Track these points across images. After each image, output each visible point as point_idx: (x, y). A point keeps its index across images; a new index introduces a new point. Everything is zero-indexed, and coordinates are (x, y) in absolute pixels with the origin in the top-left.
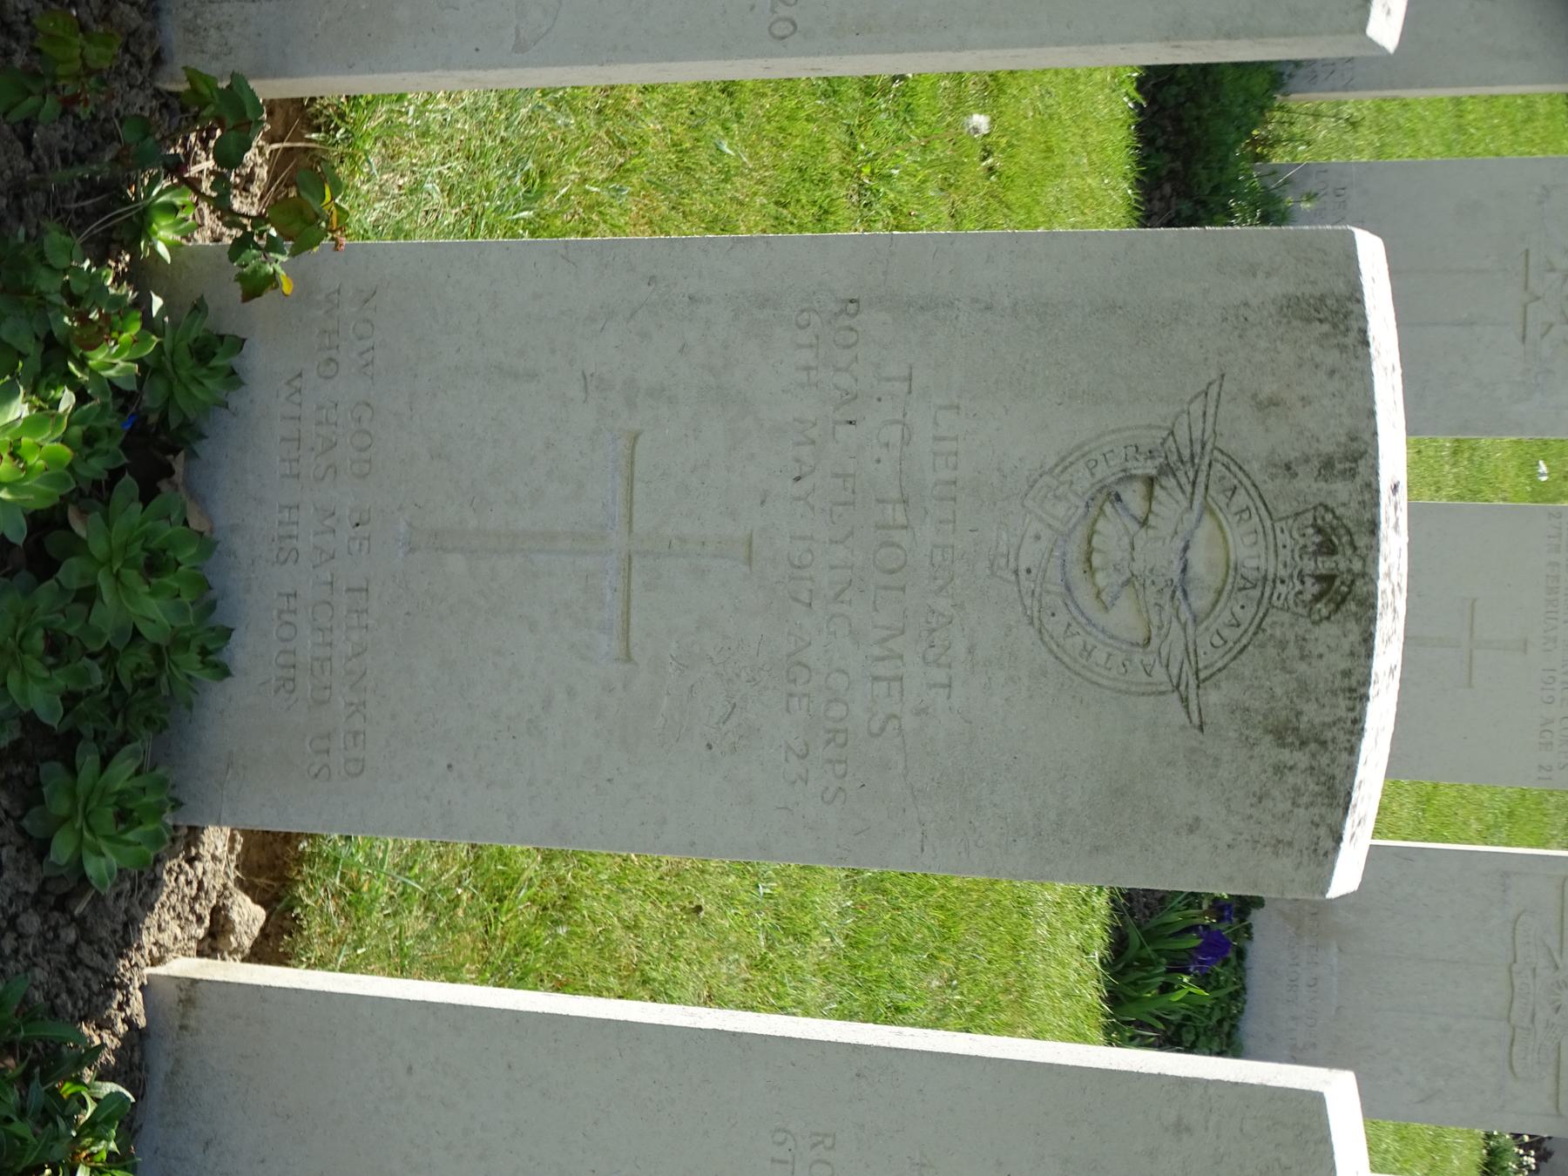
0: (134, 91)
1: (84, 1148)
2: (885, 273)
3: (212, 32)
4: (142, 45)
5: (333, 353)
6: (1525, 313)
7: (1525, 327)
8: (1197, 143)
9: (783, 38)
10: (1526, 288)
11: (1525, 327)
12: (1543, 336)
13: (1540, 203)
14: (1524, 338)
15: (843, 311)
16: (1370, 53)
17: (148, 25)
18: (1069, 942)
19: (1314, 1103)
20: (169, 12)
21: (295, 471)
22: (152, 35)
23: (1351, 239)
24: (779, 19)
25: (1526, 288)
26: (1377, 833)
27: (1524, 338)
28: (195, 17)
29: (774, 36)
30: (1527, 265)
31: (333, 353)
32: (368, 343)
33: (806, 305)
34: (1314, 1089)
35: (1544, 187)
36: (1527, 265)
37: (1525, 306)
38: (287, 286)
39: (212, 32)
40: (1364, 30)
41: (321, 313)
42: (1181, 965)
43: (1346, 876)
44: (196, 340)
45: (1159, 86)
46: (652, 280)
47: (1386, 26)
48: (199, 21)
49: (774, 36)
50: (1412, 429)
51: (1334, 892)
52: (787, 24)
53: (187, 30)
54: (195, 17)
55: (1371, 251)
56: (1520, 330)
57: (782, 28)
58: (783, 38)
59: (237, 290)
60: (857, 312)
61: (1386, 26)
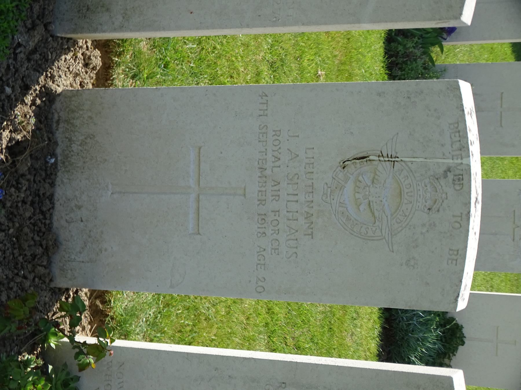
0: (43, 292)
2: (295, 375)
3: (69, 271)
4: (45, 277)
5: (110, 382)
6: (514, 231)
7: (514, 236)
8: (409, 54)
9: (260, 292)
10: (514, 223)
11: (514, 236)
14: (514, 240)
15: (280, 386)
16: (464, 25)
17: (48, 271)
20: (55, 263)
22: (49, 274)
23: (458, 82)
24: (259, 286)
25: (514, 223)
26: (471, 290)
27: (514, 240)
28: (64, 265)
29: (257, 292)
31: (110, 382)
32: (121, 380)
33: (268, 383)
36: (514, 216)
37: (514, 229)
38: (93, 366)
39: (69, 271)
40: (460, 18)
41: (106, 368)
43: (462, 305)
44: (63, 381)
45: (392, 38)
46: (216, 369)
48: (65, 267)
49: (257, 292)
50: (476, 269)
51: (458, 310)
52: (262, 288)
53: (61, 270)
54: (64, 265)
55: (466, 88)
57: (260, 289)
58: (260, 292)
59: (77, 368)
60: (285, 387)
61: (467, 16)
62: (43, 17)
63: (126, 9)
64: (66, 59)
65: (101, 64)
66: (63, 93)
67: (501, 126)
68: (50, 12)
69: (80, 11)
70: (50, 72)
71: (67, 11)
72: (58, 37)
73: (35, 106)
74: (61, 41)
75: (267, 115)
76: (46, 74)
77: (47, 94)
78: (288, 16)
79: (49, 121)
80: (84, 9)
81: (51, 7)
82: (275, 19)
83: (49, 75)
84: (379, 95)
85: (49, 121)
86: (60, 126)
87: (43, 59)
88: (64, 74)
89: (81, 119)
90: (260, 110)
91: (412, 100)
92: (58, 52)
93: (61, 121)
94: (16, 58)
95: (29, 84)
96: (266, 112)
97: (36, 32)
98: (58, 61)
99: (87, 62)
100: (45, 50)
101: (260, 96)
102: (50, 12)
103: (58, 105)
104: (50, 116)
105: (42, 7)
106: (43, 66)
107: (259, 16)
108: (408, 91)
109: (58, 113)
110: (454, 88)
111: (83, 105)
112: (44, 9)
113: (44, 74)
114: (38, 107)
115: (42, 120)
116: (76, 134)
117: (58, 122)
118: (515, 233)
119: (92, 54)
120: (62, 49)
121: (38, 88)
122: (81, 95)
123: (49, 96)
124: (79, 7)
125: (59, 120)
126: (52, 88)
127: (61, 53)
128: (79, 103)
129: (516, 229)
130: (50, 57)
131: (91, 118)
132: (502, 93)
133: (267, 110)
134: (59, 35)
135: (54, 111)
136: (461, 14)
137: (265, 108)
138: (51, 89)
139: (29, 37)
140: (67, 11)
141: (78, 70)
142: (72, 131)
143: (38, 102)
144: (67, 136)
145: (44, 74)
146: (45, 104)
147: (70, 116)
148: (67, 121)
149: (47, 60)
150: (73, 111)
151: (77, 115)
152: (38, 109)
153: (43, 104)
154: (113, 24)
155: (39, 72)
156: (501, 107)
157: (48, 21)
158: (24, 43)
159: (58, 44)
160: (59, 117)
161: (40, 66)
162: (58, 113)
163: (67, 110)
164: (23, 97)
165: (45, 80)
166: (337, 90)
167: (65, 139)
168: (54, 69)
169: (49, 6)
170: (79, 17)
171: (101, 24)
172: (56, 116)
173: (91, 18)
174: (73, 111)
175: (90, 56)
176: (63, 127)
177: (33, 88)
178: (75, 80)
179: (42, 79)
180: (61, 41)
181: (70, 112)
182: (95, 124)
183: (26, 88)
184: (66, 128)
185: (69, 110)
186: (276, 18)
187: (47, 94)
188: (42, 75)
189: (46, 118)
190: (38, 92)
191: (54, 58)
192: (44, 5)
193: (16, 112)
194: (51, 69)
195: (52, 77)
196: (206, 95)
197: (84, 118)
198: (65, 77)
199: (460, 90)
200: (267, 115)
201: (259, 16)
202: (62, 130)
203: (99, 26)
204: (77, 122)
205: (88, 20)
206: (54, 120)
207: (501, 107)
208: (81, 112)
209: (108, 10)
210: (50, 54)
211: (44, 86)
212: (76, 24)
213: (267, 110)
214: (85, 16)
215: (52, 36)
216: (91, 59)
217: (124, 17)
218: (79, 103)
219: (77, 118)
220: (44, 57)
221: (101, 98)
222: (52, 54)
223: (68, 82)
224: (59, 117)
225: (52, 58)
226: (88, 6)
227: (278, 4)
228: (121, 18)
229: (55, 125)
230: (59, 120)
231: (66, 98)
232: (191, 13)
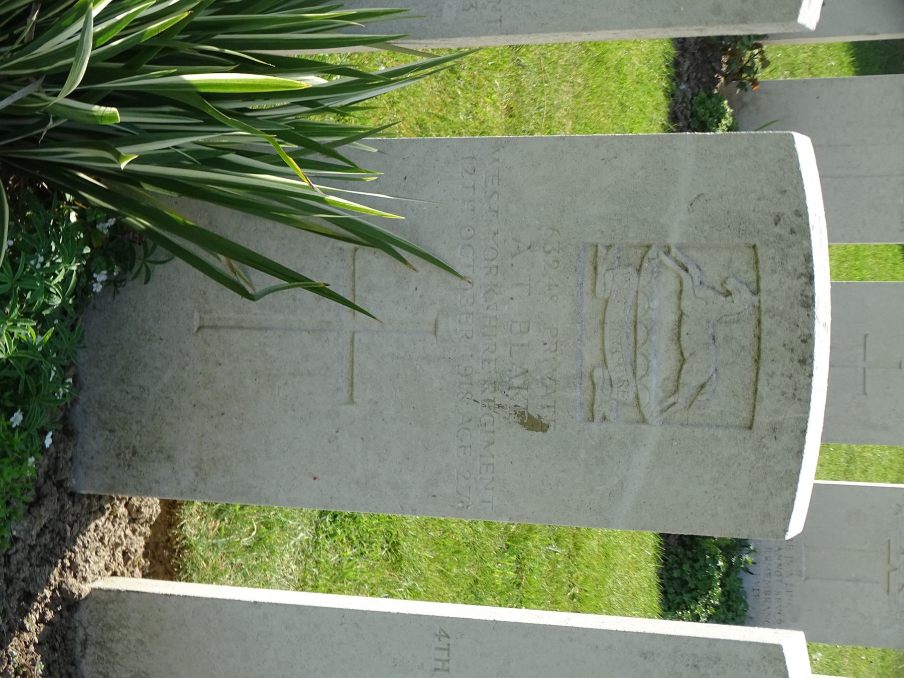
1: (177, 543)
8: (709, 80)
10: (889, 562)
12: (899, 591)
13: (896, 514)
18: (637, 561)
19: (774, 656)
21: (445, 668)
23: (792, 141)
26: (817, 477)
30: (889, 549)
34: (776, 643)
35: (898, 505)
36: (889, 549)
37: (889, 573)
42: (695, 573)
43: (796, 526)
47: (810, 15)
50: (831, 238)
51: (789, 536)
55: (803, 145)
56: (886, 587)
61: (810, 15)
62: (55, 473)
63: (201, 460)
64: (96, 526)
65: (159, 510)
66: (93, 594)
67: (865, 394)
68: (67, 463)
69: (120, 454)
70: (70, 559)
71: (98, 452)
72: (83, 495)
73: (44, 623)
74: (87, 502)
75: (448, 670)
76: (62, 563)
77: (64, 599)
78: (484, 501)
79: (69, 643)
80: (127, 452)
81: (69, 454)
82: (460, 505)
83: (68, 564)
84: (644, 655)
85: (69, 643)
86: (88, 651)
87: (56, 545)
88: (94, 553)
89: (126, 642)
90: (437, 660)
91: (702, 671)
92: (83, 520)
93: (89, 643)
94: (9, 562)
95: (32, 591)
96: (447, 664)
97: (43, 509)
98: (84, 535)
99: (134, 516)
100: (60, 525)
101: (436, 635)
102: (67, 463)
103: (83, 614)
104: (70, 635)
105: (54, 455)
106: (58, 551)
107: (434, 496)
108: (694, 655)
109: (85, 629)
110: (775, 659)
111: (128, 619)
112: (57, 458)
113: (59, 565)
114: (50, 624)
115: (57, 645)
116: (117, 667)
117: (84, 644)
118: (891, 581)
119: (143, 503)
120: (90, 513)
121: (48, 593)
122: (124, 601)
123: (68, 603)
124: (119, 448)
125: (86, 641)
126: (74, 590)
127: (88, 520)
128: (120, 615)
129: (892, 574)
130: (69, 534)
131: (142, 642)
132: (866, 336)
133: (448, 661)
134: (83, 492)
135: (77, 624)
136: (797, 16)
137: (445, 657)
138: (71, 592)
139: (31, 522)
140: (98, 452)
141: (120, 537)
142: (108, 661)
143: (50, 615)
144: (100, 669)
145: (59, 565)
146: (62, 616)
147: (105, 636)
148: (101, 645)
149: (64, 539)
150: (111, 628)
151: (117, 635)
152: (48, 628)
153: (58, 618)
154: (179, 484)
155: (50, 562)
156: (865, 360)
157: (64, 477)
158: (22, 535)
159: (82, 507)
160: (86, 635)
161: (52, 552)
162: (85, 629)
163: (100, 624)
164: (23, 619)
165: (61, 575)
166: (571, 640)
167: (96, 675)
168: (77, 550)
169: (65, 452)
170: (119, 465)
171: (157, 482)
172: (81, 634)
173: (140, 469)
174: (111, 628)
175: (140, 507)
176: (94, 653)
177: (40, 595)
178: (113, 555)
179: (55, 577)
180: (87, 502)
181: (105, 629)
182: (149, 655)
183: (29, 597)
184: (99, 655)
185: (103, 625)
186: (462, 502)
187: (64, 599)
188: (56, 566)
189: (64, 638)
190: (48, 600)
191: (75, 534)
192: (57, 453)
193: (10, 650)
194: (71, 551)
195: (74, 568)
196: (342, 624)
197: (129, 641)
198: (96, 559)
199: (785, 662)
200: (448, 670)
201: (434, 496)
202: (92, 658)
203: (155, 486)
204: (118, 648)
205: (134, 472)
206: (78, 640)
207: (865, 360)
208: (125, 631)
209: (168, 458)
210: (68, 528)
211: (59, 587)
212: (113, 477)
213: (448, 661)
214: (129, 465)
215: (72, 495)
216: (142, 513)
217: (197, 475)
218: (120, 615)
219: (118, 641)
220: (59, 533)
221: (159, 610)
222: (71, 526)
223: (102, 565)
224: (86, 635)
225: (72, 533)
226: (134, 447)
227: (466, 479)
228: (193, 475)
229: (79, 648)
230: (86, 641)
231: (97, 602)
232: (315, 479)
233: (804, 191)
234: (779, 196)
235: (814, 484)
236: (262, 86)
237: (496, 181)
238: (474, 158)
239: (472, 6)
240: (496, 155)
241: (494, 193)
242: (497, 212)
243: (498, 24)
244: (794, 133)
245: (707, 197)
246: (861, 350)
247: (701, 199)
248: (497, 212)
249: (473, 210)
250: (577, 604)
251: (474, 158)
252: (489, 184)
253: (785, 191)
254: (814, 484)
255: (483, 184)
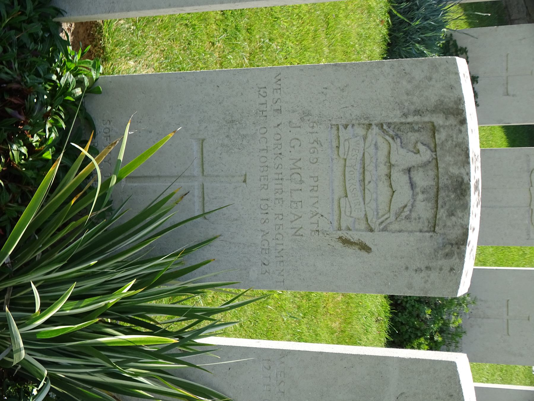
26: (476, 264)
67: (508, 335)
132: (508, 301)
156: (508, 315)
207: (508, 315)
233: (463, 396)
234: (449, 398)
235: (474, 269)
236: (157, 342)
237: (282, 375)
238: (269, 360)
239: (267, 272)
240: (283, 360)
241: (282, 381)
242: (284, 392)
243: (282, 284)
244: (457, 58)
245: (406, 395)
246: (505, 309)
247: (403, 396)
248: (284, 392)
249: (269, 391)
250: (268, 335)
251: (269, 360)
252: (279, 376)
253: (452, 395)
254: (474, 269)
255: (275, 376)
